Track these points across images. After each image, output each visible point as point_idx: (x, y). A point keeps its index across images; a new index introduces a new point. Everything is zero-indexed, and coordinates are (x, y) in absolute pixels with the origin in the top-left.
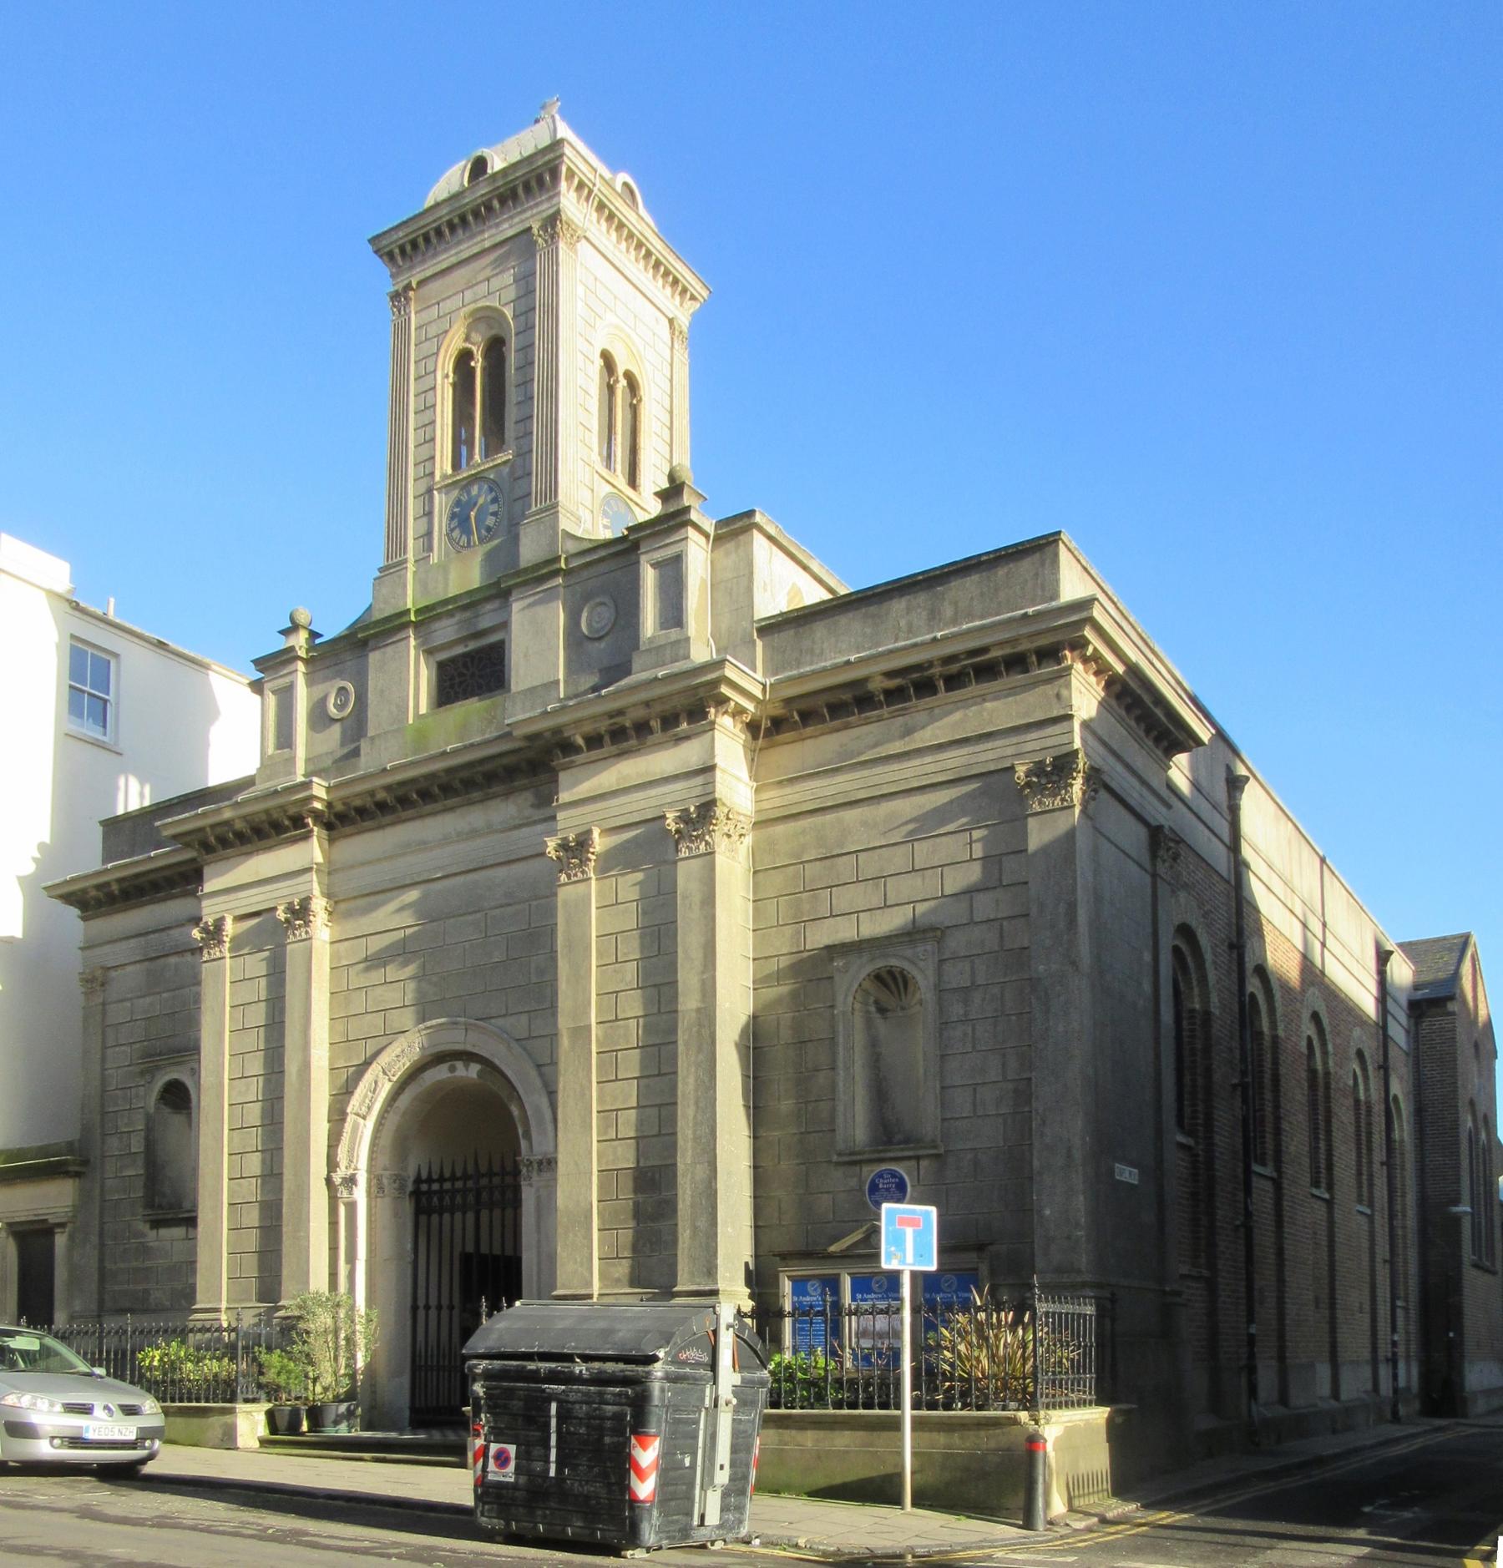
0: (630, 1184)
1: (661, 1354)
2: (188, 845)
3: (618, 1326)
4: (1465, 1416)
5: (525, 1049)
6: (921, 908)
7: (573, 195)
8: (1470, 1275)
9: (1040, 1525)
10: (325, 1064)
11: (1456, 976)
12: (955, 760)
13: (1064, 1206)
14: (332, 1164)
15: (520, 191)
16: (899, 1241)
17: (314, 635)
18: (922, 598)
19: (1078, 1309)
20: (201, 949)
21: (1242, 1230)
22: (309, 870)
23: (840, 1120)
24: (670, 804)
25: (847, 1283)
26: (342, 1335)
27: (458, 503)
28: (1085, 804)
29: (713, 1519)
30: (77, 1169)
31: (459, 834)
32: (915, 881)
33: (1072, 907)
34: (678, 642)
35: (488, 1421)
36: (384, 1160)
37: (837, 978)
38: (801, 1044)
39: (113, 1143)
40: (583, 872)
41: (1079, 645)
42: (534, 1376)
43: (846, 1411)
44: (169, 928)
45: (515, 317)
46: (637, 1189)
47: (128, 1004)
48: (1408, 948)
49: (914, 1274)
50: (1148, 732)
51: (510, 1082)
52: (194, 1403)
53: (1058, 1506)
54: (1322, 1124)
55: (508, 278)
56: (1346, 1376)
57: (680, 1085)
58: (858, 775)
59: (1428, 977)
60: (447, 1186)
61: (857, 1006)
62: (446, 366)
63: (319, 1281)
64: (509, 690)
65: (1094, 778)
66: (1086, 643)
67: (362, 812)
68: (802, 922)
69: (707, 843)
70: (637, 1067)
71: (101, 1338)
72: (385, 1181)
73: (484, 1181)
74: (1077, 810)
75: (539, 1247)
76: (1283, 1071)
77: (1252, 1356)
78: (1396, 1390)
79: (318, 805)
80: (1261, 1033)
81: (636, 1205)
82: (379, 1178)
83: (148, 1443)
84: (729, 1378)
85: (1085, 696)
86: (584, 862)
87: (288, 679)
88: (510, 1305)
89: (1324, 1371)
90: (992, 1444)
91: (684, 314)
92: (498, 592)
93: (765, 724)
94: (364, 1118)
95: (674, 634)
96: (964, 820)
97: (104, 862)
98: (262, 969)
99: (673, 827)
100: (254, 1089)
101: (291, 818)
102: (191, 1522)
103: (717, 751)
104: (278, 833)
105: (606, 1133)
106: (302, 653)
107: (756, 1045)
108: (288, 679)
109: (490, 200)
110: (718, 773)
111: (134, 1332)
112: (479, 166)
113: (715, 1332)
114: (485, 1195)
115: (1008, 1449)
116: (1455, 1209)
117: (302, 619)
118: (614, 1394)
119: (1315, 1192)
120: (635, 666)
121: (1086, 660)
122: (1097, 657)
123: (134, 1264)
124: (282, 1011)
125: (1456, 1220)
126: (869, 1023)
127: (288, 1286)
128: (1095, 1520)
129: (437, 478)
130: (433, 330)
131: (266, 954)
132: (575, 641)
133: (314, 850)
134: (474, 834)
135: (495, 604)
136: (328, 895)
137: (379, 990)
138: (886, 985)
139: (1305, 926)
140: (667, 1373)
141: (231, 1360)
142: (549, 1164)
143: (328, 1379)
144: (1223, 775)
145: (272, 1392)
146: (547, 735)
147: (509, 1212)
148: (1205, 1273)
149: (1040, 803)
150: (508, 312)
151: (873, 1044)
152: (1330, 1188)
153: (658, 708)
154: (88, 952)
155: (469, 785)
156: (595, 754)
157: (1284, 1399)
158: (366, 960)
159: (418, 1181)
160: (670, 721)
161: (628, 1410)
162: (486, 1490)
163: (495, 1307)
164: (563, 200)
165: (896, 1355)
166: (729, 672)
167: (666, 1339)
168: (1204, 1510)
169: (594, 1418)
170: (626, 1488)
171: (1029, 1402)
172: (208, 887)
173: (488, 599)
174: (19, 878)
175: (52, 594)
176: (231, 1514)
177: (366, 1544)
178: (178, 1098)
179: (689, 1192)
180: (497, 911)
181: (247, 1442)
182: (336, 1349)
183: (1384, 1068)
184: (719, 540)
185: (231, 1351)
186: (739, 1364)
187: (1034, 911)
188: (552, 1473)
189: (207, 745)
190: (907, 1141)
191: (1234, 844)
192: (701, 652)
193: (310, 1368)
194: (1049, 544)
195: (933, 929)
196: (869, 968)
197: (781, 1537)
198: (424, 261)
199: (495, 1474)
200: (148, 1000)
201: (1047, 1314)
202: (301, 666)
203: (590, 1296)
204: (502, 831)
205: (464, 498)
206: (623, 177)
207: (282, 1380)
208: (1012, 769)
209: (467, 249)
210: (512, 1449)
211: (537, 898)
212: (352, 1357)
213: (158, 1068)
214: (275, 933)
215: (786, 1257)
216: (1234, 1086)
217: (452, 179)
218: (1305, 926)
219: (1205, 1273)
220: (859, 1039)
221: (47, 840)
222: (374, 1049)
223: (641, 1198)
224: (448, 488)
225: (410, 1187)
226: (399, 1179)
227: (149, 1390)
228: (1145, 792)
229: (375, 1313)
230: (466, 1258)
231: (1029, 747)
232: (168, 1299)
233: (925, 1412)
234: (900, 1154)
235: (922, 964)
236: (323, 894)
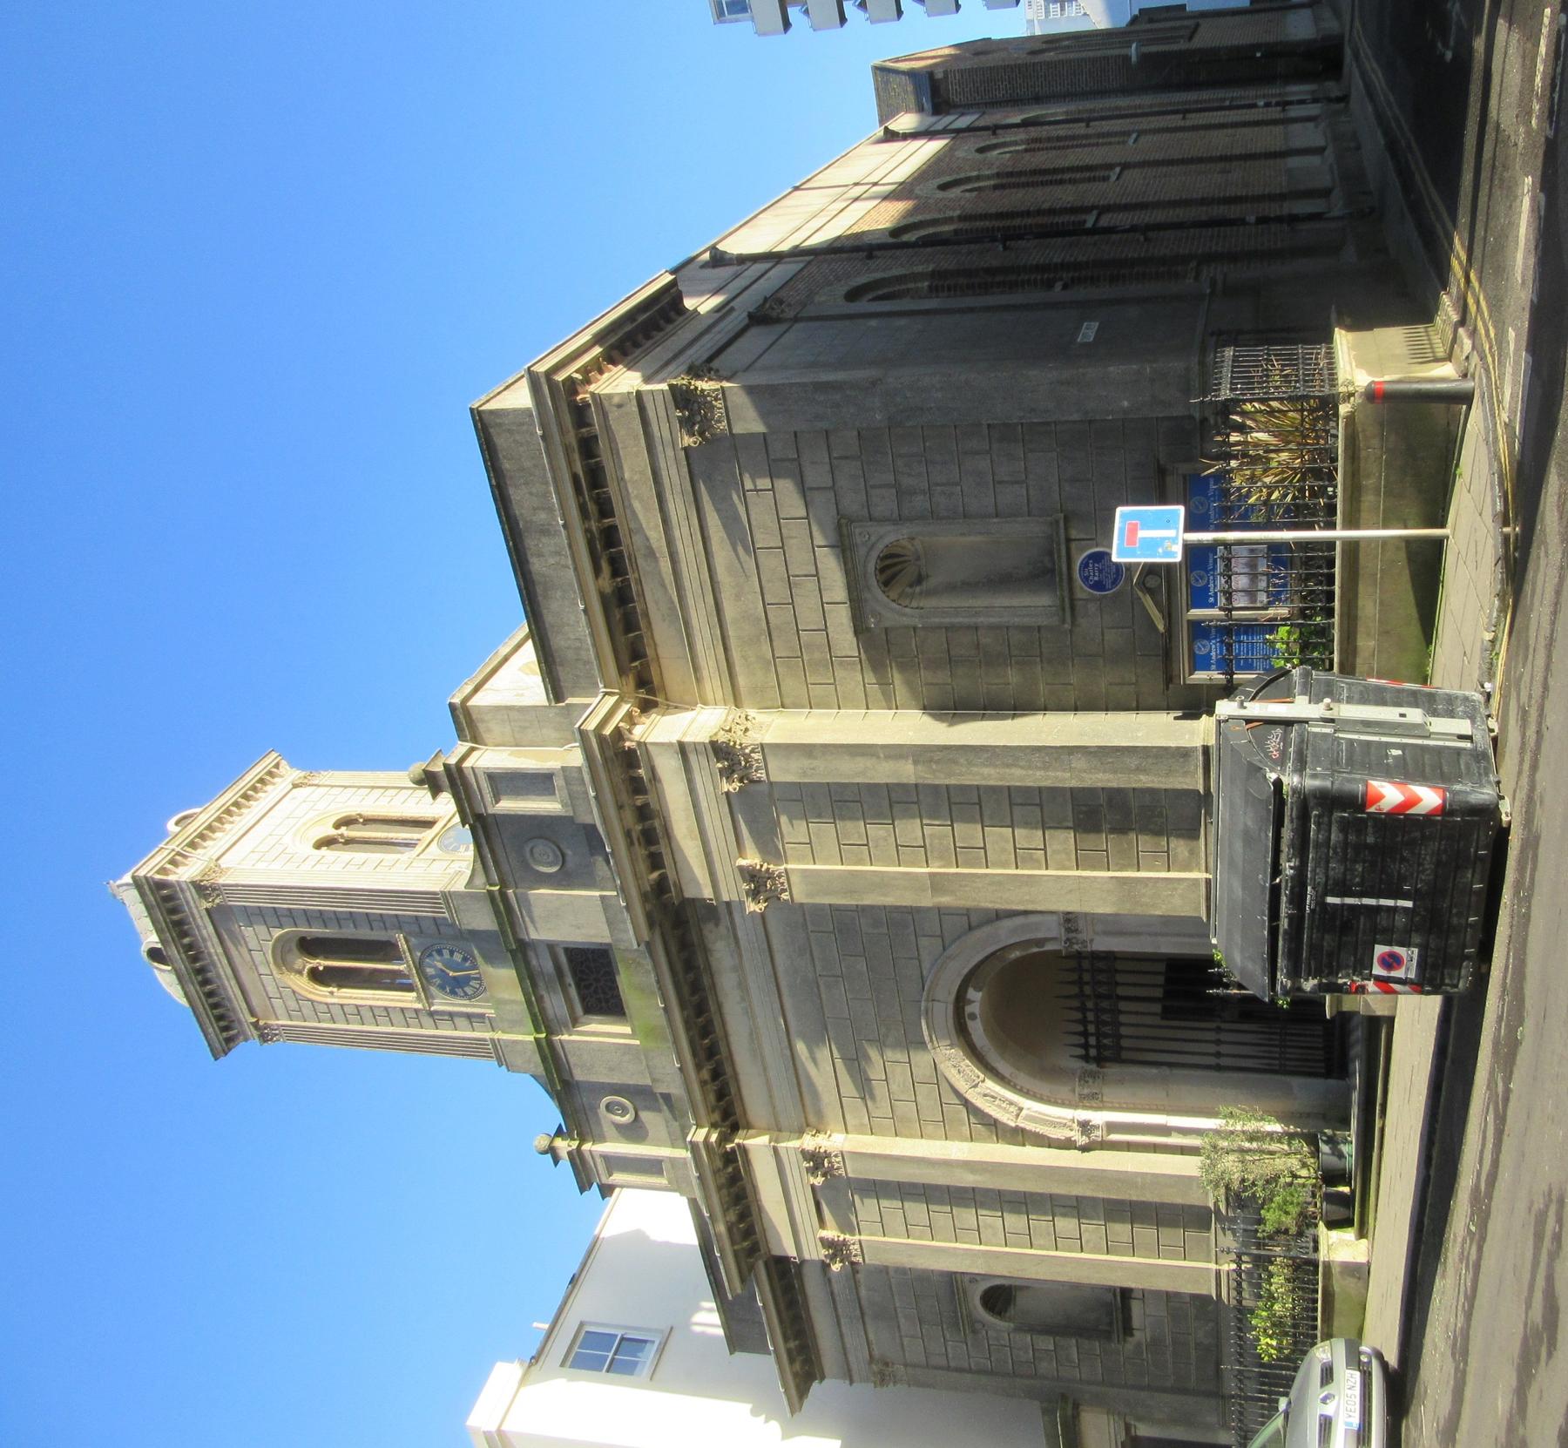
0: (1092, 836)
1: (1273, 776)
2: (751, 1268)
3: (1241, 827)
4: (1342, 37)
5: (954, 941)
6: (819, 539)
7: (180, 870)
8: (1198, 42)
9: (1468, 385)
10: (966, 1145)
11: (911, 74)
12: (678, 507)
13: (1120, 387)
14: (1067, 1144)
15: (175, 917)
16: (1153, 544)
17: (559, 1133)
18: (530, 543)
19: (1228, 364)
20: (852, 1263)
21: (1150, 234)
22: (775, 1149)
23: (1026, 621)
24: (715, 787)
25: (1196, 613)
26: (1247, 1145)
27: (442, 988)
28: (720, 378)
29: (1464, 727)
30: (1070, 1406)
32: (792, 544)
33: (820, 387)
34: (566, 779)
35: (1347, 976)
36: (1064, 1091)
37: (888, 624)
38: (951, 661)
39: (1046, 1367)
40: (780, 876)
41: (571, 386)
42: (1297, 921)
43: (1337, 604)
44: (832, 1293)
45: (281, 927)
46: (1096, 829)
47: (906, 1341)
48: (884, 117)
49: (1188, 529)
50: (660, 329)
51: (987, 958)
52: (1319, 1305)
53: (1447, 370)
54: (1049, 178)
55: (248, 932)
56: (1298, 143)
57: (992, 783)
58: (691, 602)
59: (911, 99)
60: (1092, 1028)
61: (914, 604)
62: (322, 994)
63: (1189, 1166)
64: (609, 945)
65: (695, 372)
66: (570, 381)
67: (722, 1094)
68: (832, 659)
69: (753, 751)
70: (972, 826)
71: (1247, 1398)
72: (1086, 1091)
73: (1088, 990)
74: (726, 384)
75: (1156, 934)
76: (993, 210)
77: (1279, 219)
78: (1315, 101)
79: (714, 1137)
80: (956, 232)
81: (1113, 830)
82: (1083, 1097)
83: (1364, 1359)
84: (1300, 707)
85: (622, 382)
86: (770, 875)
87: (599, 1161)
88: (1219, 965)
89: (1294, 162)
90: (1375, 442)
91: (290, 774)
92: (520, 952)
93: (642, 694)
94: (1021, 1109)
95: (558, 782)
96: (735, 497)
97: (767, 1352)
98: (871, 1203)
99: (737, 785)
100: (991, 1219)
101: (726, 1165)
102: (1461, 1319)
103: (666, 740)
104: (741, 1179)
105: (1038, 861)
106: (575, 1144)
107: (951, 706)
109: (184, 946)
110: (686, 739)
111: (1241, 1364)
112: (155, 954)
113: (1248, 721)
114: (1102, 990)
115: (1382, 425)
116: (1134, 59)
117: (543, 1142)
118: (1318, 830)
119: (1114, 178)
120: (588, 820)
121: (588, 381)
122: (585, 370)
124: (914, 1185)
125: (1145, 58)
126: (929, 593)
127: (1194, 1198)
128: (1461, 331)
129: (419, 1006)
130: (292, 1004)
132: (565, 878)
133: (756, 1143)
134: (743, 986)
135: (531, 954)
136: (800, 1132)
137: (894, 1087)
138: (893, 577)
139: (856, 199)
140: (1295, 771)
141: (1272, 1263)
142: (1070, 921)
143: (1294, 1162)
144: (709, 272)
145: (1306, 1221)
146: (648, 907)
147: (1119, 966)
148: (1193, 264)
149: (719, 421)
150: (277, 933)
151: (952, 588)
152: (1110, 167)
153: (624, 797)
154: (855, 1377)
156: (667, 861)
157: (1326, 193)
158: (863, 1099)
159: (1086, 1058)
160: (637, 787)
161: (1337, 815)
162: (1424, 983)
163: (1218, 981)
164: (184, 878)
165: (1274, 547)
166: (591, 726)
167: (1255, 771)
168: (1449, 224)
169: (1345, 853)
170: (1428, 817)
171: (1328, 405)
172: (791, 1252)
173: (527, 963)
174: (783, 1438)
175: (523, 1381)
176: (1450, 1270)
177: (1491, 1118)
178: (1000, 1297)
179: (1100, 776)
181: (1367, 1252)
182: (1262, 1152)
183: (994, 129)
184: (476, 739)
185: (1262, 1262)
186: (1287, 696)
187: (824, 425)
188: (1409, 904)
189: (667, 1244)
190: (1051, 553)
191: (773, 258)
192: (574, 757)
193: (1282, 1180)
194: (481, 419)
195: (839, 526)
196: (877, 591)
197: (1483, 658)
198: (234, 1010)
199: (1409, 969)
200: (902, 1321)
201: (1232, 390)
202: (587, 1147)
203: (1208, 882)
204: (740, 956)
205: (438, 981)
206: (171, 826)
207: (1294, 1210)
208: (686, 450)
209: (223, 969)
210: (1380, 950)
211: (805, 924)
212: (1270, 1135)
213: (969, 1315)
214: (838, 1189)
215: (1169, 678)
216: (1005, 248)
217: (165, 978)
218: (856, 199)
219: (1193, 264)
220: (946, 602)
221: (749, 1406)
222: (953, 1096)
223: (1106, 826)
224: (429, 997)
225: (1093, 1067)
226: (1085, 1077)
227: (1305, 1353)
228: (717, 329)
229: (1223, 1109)
230: (1167, 1013)
231: (666, 434)
232: (1204, 1323)
233: (1339, 518)
234: (1064, 559)
235: (873, 539)
236: (800, 1137)
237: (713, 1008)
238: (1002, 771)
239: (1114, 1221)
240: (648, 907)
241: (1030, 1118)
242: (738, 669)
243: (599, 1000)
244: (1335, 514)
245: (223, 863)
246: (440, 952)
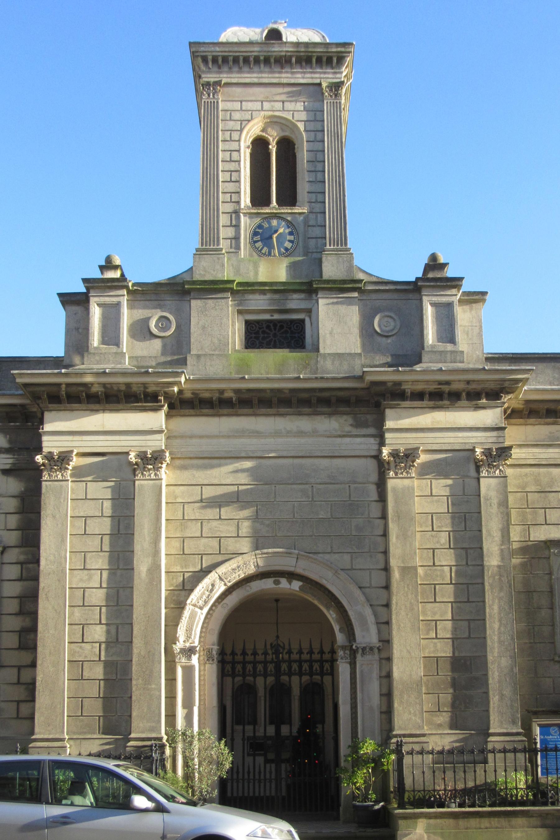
0: (448, 667)
15: (314, 60)
31: (288, 432)
40: (407, 473)
69: (500, 470)
81: (453, 679)
86: (63, 469)
94: (201, 608)
108: (115, 300)
109: (291, 57)
117: (117, 261)
131: (112, 484)
134: (301, 433)
137: (215, 523)
146: (390, 384)
173: (295, 291)
179: (496, 674)
209: (267, 77)
211: (355, 483)
214: (123, 473)
223: (456, 675)
237: (282, 410)
238: (496, 616)
240: (390, 384)
241: (193, 616)
242: (518, 470)
243: (257, 333)
244: (438, 807)
246: (291, 233)
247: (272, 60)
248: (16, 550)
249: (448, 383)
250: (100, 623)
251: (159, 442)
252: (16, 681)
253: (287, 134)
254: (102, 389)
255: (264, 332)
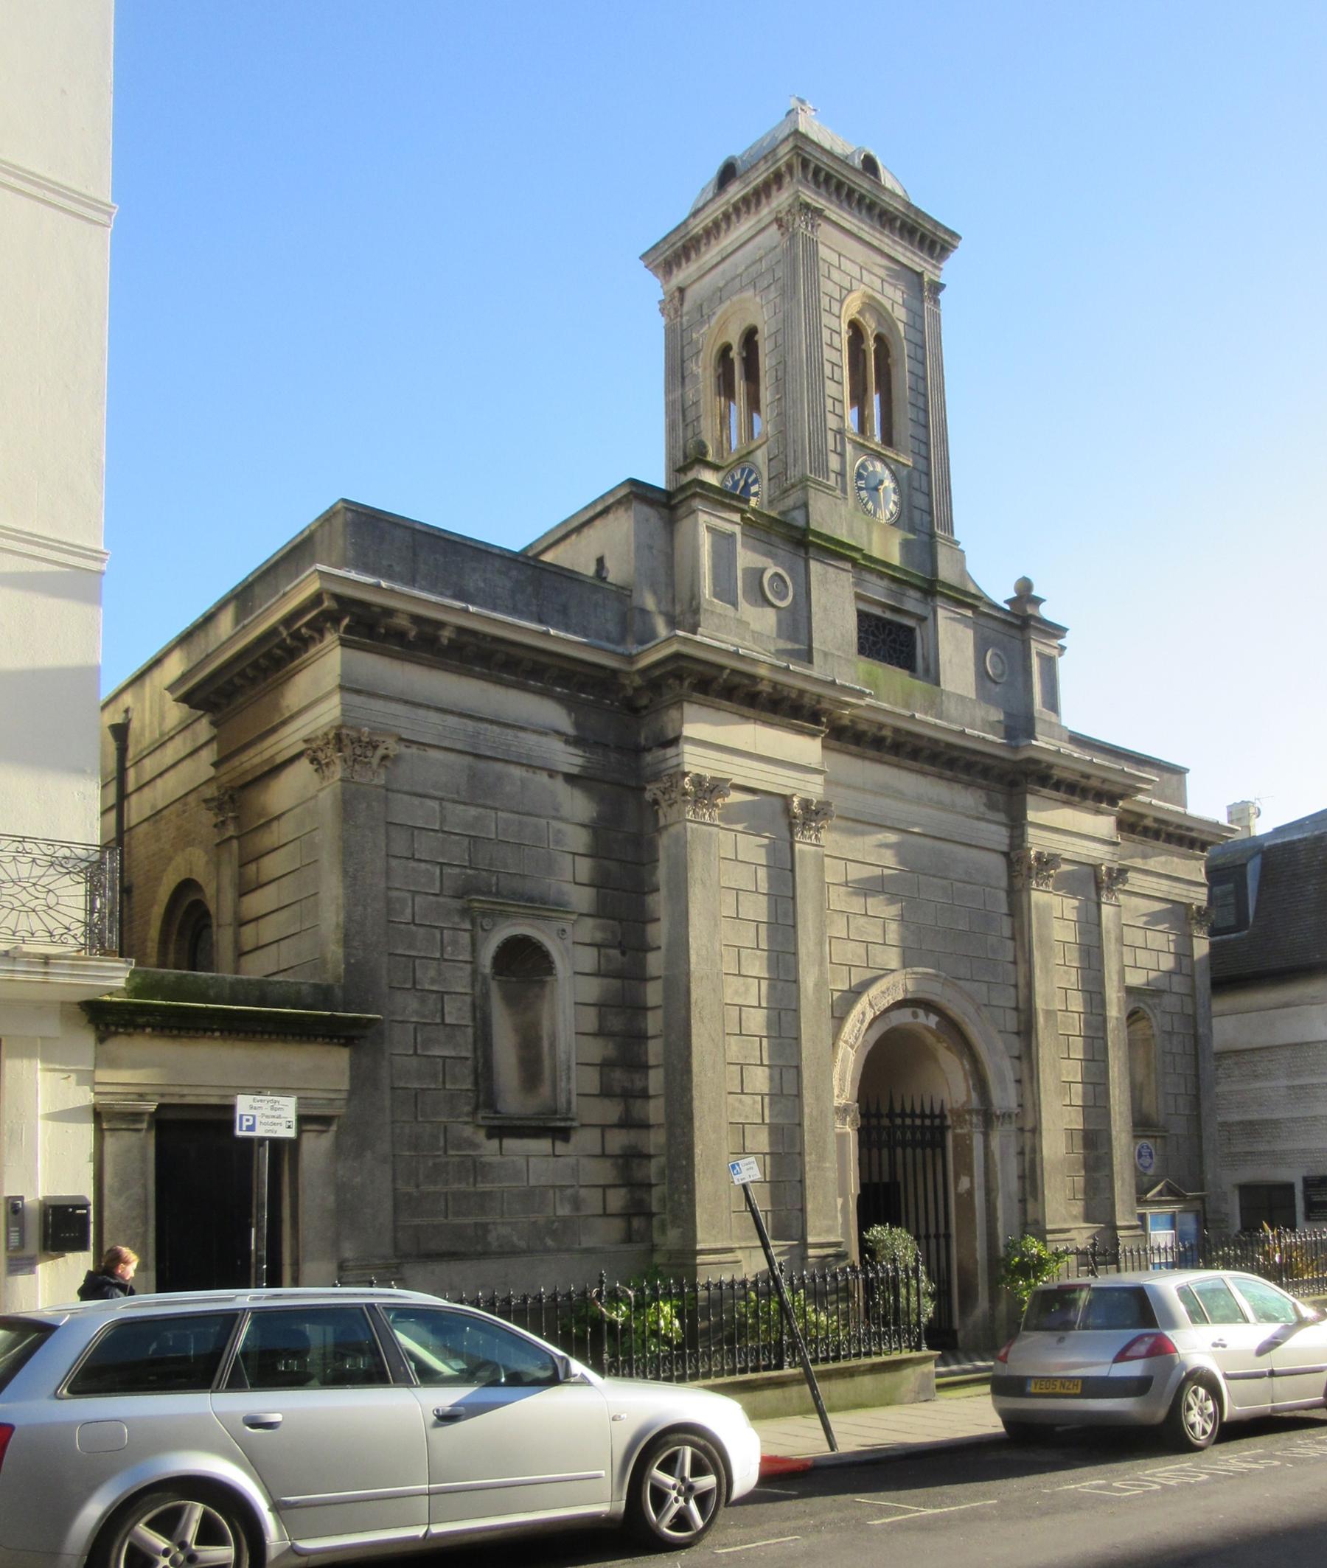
81: (1085, 1158)
109: (896, 218)
123: (455, 1186)
131: (766, 841)
147: (939, 1151)
155: (951, 764)
180: (960, 885)
209: (866, 231)
239: (770, 1134)
241: (844, 1060)
245: (825, 228)
247: (877, 211)
248: (590, 922)
249: (1088, 777)
250: (762, 1065)
251: (814, 788)
252: (598, 1151)
253: (884, 331)
254: (769, 690)
255: (873, 634)
